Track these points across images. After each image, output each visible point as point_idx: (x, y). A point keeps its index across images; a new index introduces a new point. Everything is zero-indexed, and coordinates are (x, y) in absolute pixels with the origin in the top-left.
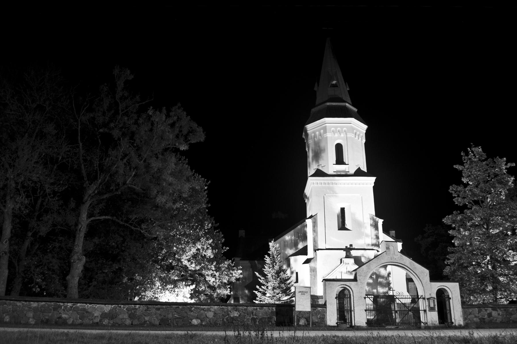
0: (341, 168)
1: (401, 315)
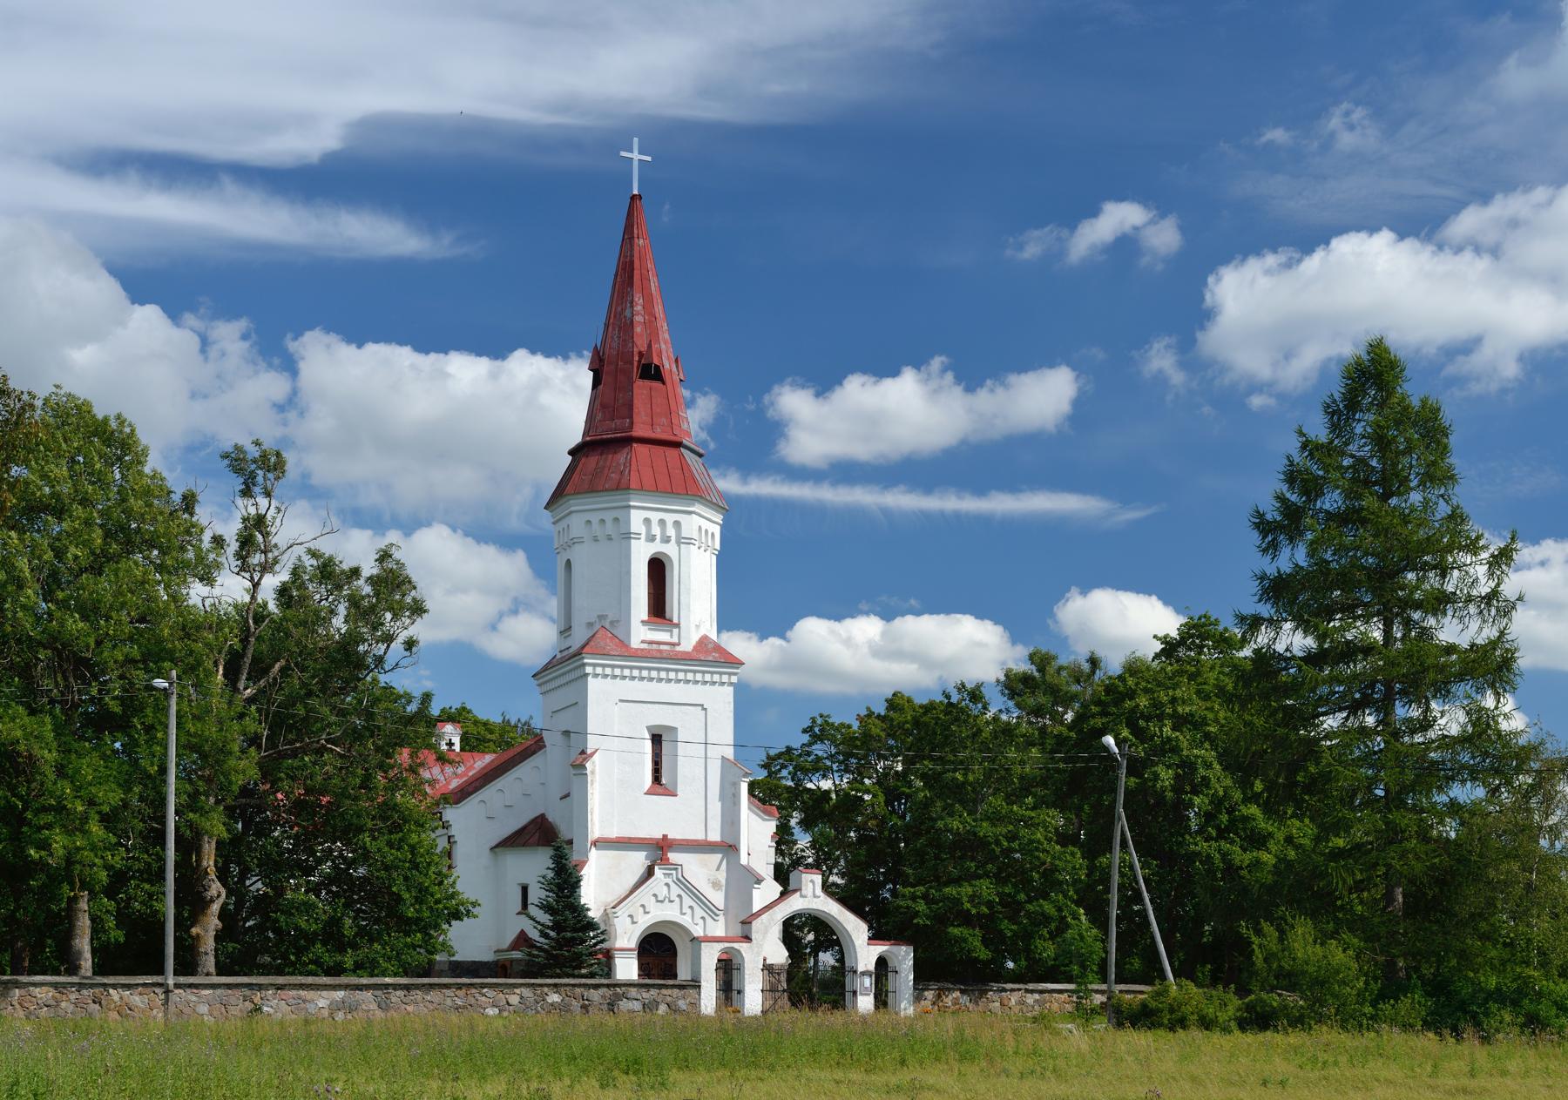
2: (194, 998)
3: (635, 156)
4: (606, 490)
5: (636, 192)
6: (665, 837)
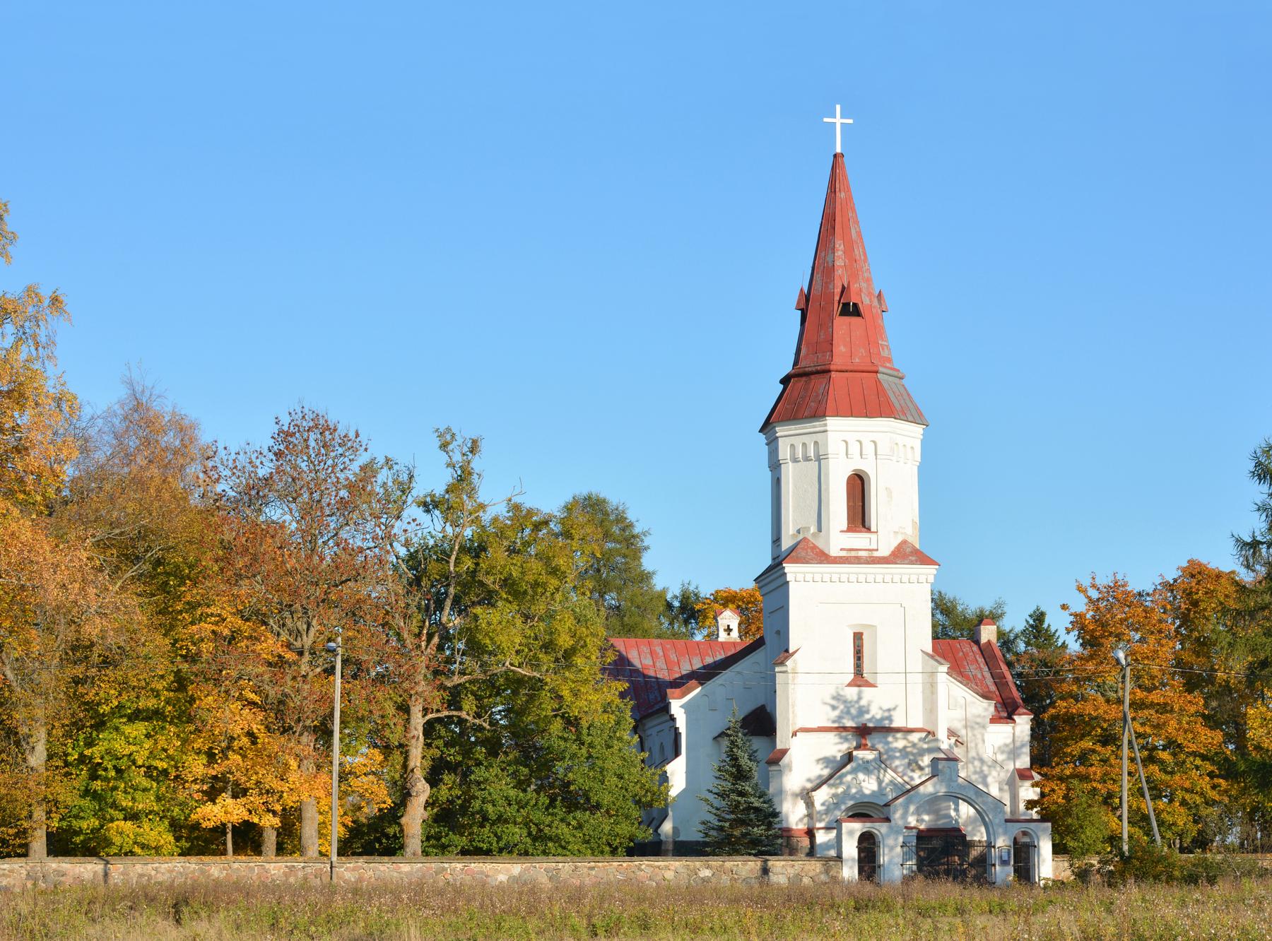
0: (859, 541)
1: (830, 265)
3: (838, 121)
4: (806, 418)
5: (839, 150)
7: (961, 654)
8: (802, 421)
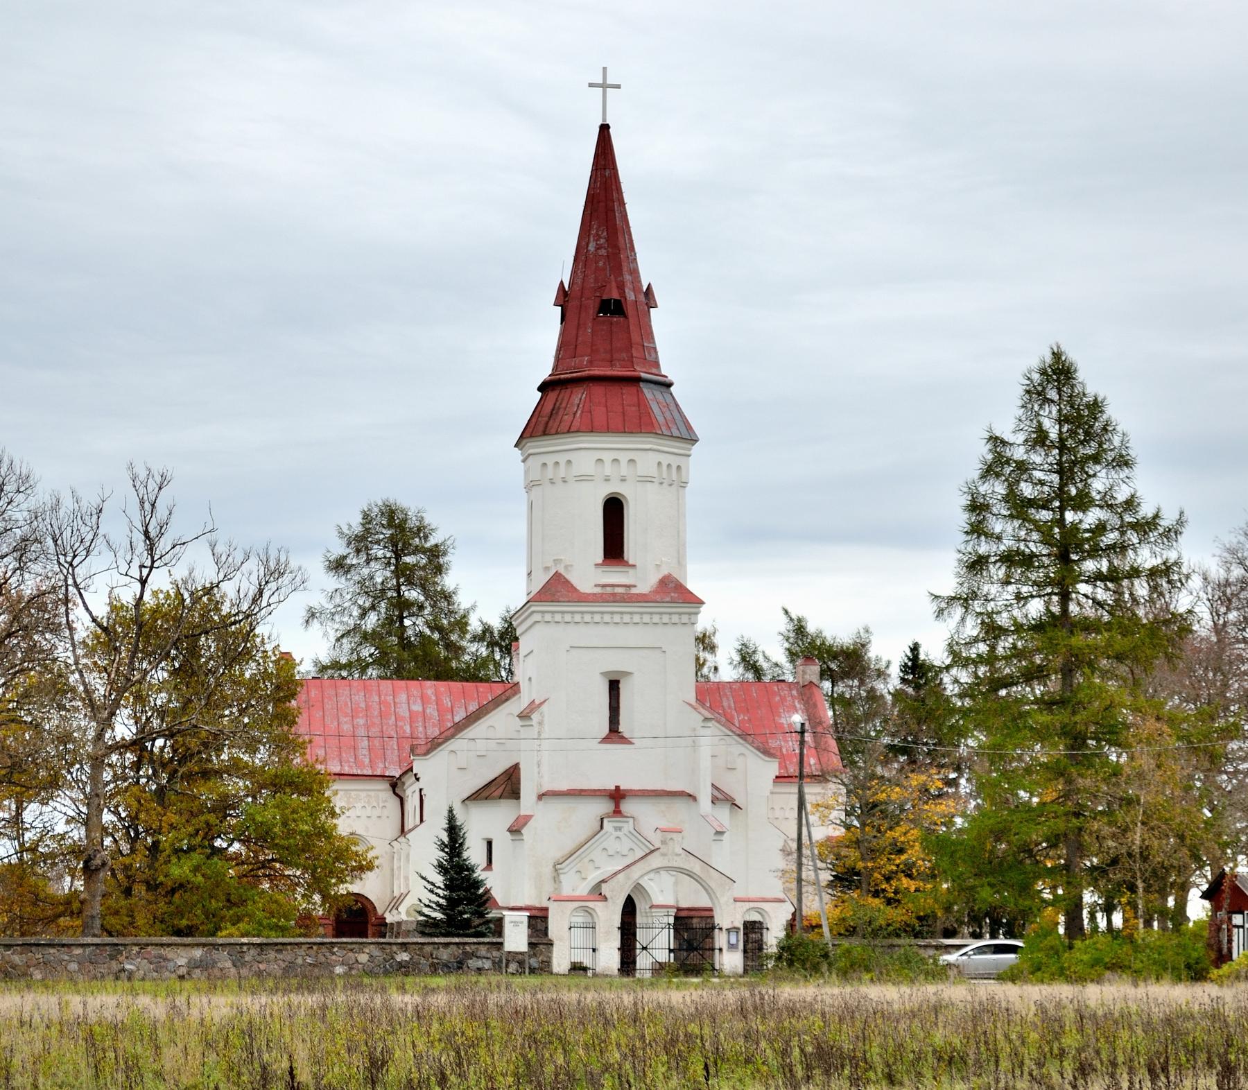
0: (615, 576)
2: (66, 958)
6: (617, 788)
7: (777, 698)
8: (556, 436)
